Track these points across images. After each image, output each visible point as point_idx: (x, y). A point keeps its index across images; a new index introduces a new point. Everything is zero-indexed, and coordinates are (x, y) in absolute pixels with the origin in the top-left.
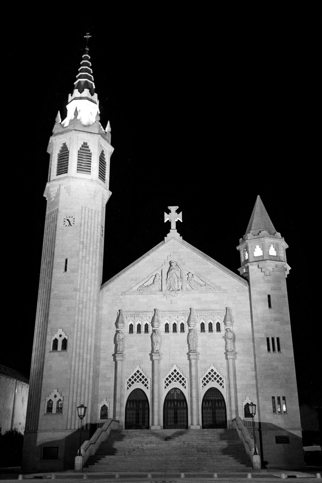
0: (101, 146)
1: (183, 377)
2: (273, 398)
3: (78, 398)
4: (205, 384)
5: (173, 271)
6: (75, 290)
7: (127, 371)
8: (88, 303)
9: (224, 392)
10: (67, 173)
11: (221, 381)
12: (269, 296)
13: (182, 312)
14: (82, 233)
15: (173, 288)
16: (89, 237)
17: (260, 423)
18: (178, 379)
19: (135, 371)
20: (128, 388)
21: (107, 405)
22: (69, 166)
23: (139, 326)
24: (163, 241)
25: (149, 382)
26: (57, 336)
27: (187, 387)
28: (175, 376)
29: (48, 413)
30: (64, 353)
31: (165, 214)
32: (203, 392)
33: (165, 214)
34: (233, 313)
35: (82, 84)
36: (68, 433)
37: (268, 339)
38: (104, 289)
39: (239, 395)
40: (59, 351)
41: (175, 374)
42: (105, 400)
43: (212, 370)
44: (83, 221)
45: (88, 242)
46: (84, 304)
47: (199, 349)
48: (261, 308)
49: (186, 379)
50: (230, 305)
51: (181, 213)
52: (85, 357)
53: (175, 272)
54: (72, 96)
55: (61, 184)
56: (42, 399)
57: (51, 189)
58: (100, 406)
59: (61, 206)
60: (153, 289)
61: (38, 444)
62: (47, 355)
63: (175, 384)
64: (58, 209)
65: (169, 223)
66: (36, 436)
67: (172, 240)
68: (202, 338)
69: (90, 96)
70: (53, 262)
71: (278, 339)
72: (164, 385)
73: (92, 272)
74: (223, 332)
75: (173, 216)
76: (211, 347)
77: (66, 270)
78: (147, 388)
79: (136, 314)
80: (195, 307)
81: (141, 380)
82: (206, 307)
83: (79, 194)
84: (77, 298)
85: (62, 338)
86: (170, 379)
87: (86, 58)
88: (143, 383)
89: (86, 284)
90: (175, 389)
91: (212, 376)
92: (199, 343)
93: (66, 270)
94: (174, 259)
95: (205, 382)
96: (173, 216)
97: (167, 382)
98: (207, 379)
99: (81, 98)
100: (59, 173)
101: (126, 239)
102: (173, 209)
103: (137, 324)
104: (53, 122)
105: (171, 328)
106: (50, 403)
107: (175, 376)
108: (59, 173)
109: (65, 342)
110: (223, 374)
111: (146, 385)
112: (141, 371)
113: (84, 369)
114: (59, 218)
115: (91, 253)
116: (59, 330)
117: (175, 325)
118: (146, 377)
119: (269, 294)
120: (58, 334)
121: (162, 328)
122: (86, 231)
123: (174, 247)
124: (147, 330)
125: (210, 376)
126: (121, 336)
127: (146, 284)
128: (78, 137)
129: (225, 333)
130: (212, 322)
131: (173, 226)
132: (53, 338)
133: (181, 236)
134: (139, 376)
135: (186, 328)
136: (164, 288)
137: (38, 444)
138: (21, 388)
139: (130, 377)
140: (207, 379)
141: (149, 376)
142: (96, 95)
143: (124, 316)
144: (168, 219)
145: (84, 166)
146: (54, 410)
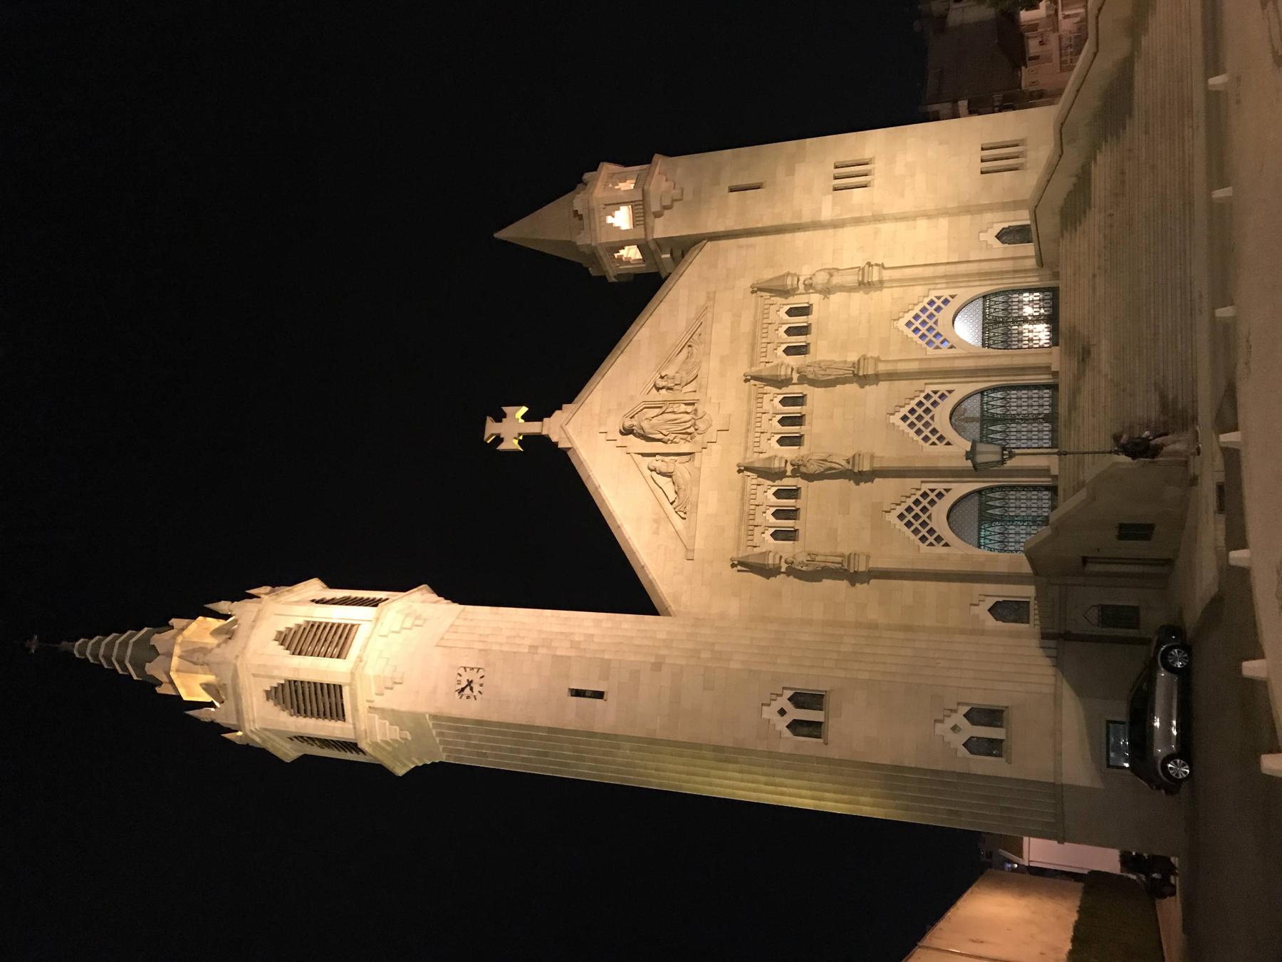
0: (304, 603)
1: (921, 398)
5: (645, 425)
10: (340, 686)
13: (753, 402)
15: (688, 425)
18: (927, 411)
19: (900, 525)
20: (946, 545)
21: (990, 602)
22: (326, 680)
24: (569, 453)
25: (932, 486)
26: (782, 724)
27: (949, 387)
29: (1005, 723)
30: (831, 701)
31: (502, 447)
33: (502, 447)
34: (768, 275)
36: (1067, 692)
38: (673, 607)
40: (827, 717)
41: (909, 517)
42: (975, 610)
47: (853, 357)
50: (746, 283)
51: (506, 409)
54: (160, 684)
55: (368, 704)
56: (959, 769)
57: (379, 738)
59: (425, 707)
60: (687, 476)
61: (1098, 785)
62: (833, 753)
64: (434, 717)
65: (527, 440)
66: (1072, 787)
67: (569, 429)
70: (575, 732)
72: (941, 447)
77: (599, 695)
78: (947, 490)
79: (748, 522)
80: (744, 368)
82: (744, 348)
84: (683, 662)
85: (789, 707)
86: (927, 432)
88: (932, 502)
91: (916, 517)
92: (835, 357)
93: (599, 695)
94: (614, 424)
95: (931, 539)
96: (512, 428)
97: (934, 439)
100: (337, 712)
101: (551, 548)
102: (492, 428)
103: (772, 520)
105: (792, 430)
106: (973, 745)
108: (337, 712)
109: (800, 700)
111: (942, 396)
114: (455, 713)
116: (765, 716)
120: (776, 719)
121: (789, 452)
125: (923, 330)
127: (672, 496)
129: (816, 292)
130: (785, 327)
132: (788, 733)
133: (560, 409)
134: (919, 417)
135: (794, 390)
136: (685, 448)
137: (1098, 785)
139: (916, 539)
140: (930, 336)
141: (913, 485)
143: (750, 551)
144: (516, 442)
145: (333, 640)
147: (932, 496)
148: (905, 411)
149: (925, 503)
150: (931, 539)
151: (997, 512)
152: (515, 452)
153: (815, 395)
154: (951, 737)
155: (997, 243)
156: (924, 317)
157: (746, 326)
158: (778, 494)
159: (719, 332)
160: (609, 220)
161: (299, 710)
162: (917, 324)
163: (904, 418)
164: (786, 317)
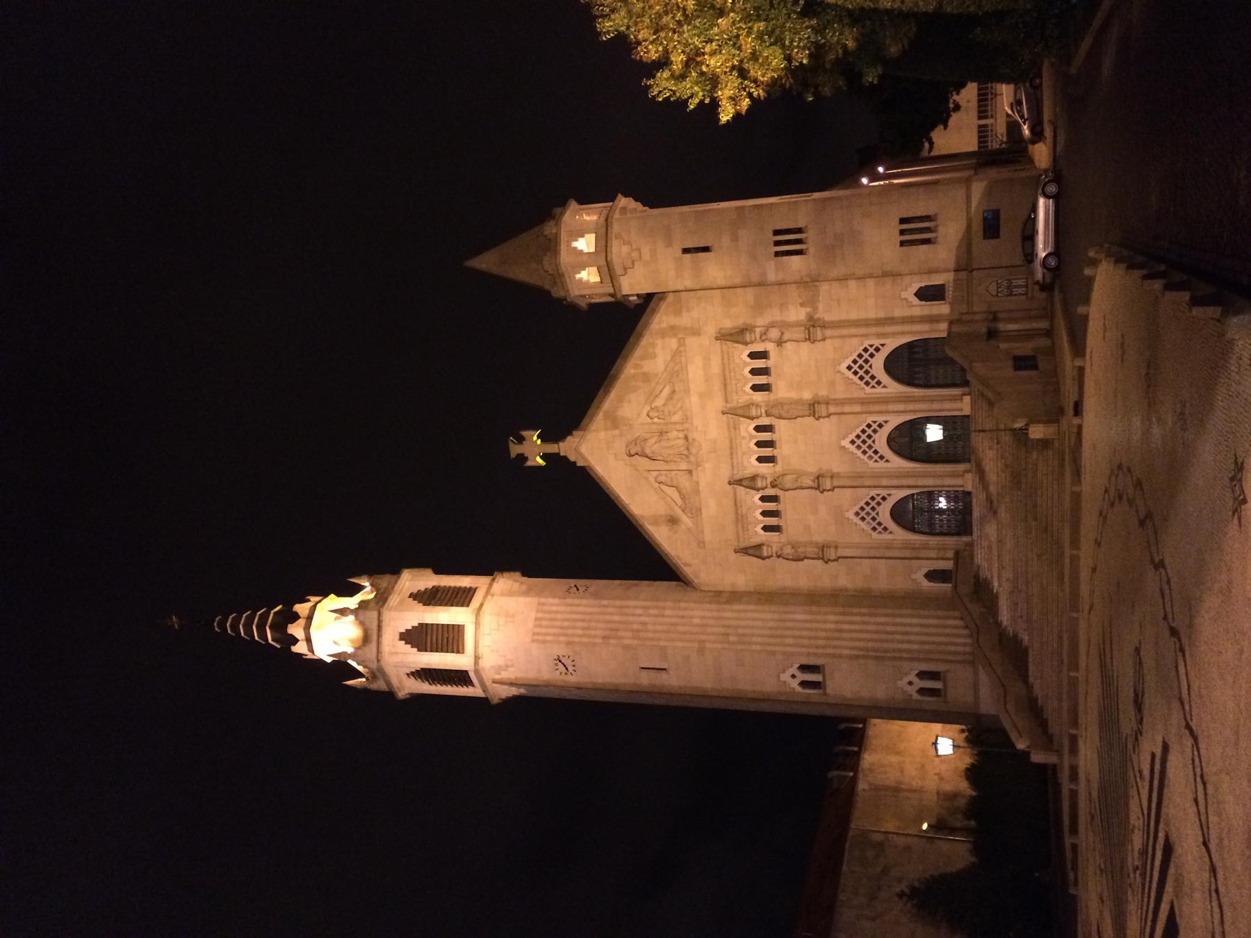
2: (902, 244)
3: (913, 638)
4: (879, 383)
6: (701, 651)
7: (858, 534)
8: (726, 623)
9: (892, 344)
11: (871, 350)
12: (686, 251)
14: (584, 640)
16: (593, 624)
17: (956, 271)
21: (925, 571)
23: (754, 372)
26: (794, 684)
28: (864, 442)
32: (893, 387)
35: (277, 635)
37: (777, 254)
39: (898, 313)
41: (855, 367)
42: (914, 576)
43: (849, 368)
44: (562, 639)
45: (602, 625)
46: (729, 631)
48: (715, 270)
49: (869, 421)
51: (525, 433)
52: (832, 626)
53: (652, 446)
58: (926, 584)
63: (884, 512)
68: (782, 391)
69: (302, 622)
71: (776, 233)
73: (663, 616)
74: (770, 347)
75: (533, 449)
76: (801, 368)
79: (740, 519)
81: (873, 509)
82: (717, 386)
83: (503, 633)
85: (797, 673)
87: (222, 625)
88: (879, 504)
89: (686, 629)
90: (890, 441)
91: (861, 367)
92: (793, 395)
97: (876, 457)
98: (867, 378)
99: (308, 640)
101: (592, 541)
103: (761, 518)
104: (364, 691)
107: (864, 442)
110: (855, 346)
111: (880, 426)
112: (857, 508)
113: (857, 627)
115: (624, 618)
117: (760, 444)
118: (860, 350)
119: (680, 252)
121: (765, 468)
122: (580, 632)
123: (599, 448)
124: (774, 499)
125: (861, 373)
126: (788, 550)
127: (679, 501)
128: (391, 653)
131: (552, 448)
138: (872, 311)
140: (867, 378)
142: (298, 608)
146: (937, 685)
147: (878, 499)
148: (852, 437)
149: (873, 504)
150: (873, 383)
151: (920, 356)
152: (540, 467)
153: (780, 425)
154: (908, 688)
155: (916, 301)
156: (861, 362)
157: (716, 368)
158: (763, 499)
159: (695, 372)
160: (575, 244)
161: (422, 648)
162: (855, 367)
163: (853, 442)
164: (748, 360)
